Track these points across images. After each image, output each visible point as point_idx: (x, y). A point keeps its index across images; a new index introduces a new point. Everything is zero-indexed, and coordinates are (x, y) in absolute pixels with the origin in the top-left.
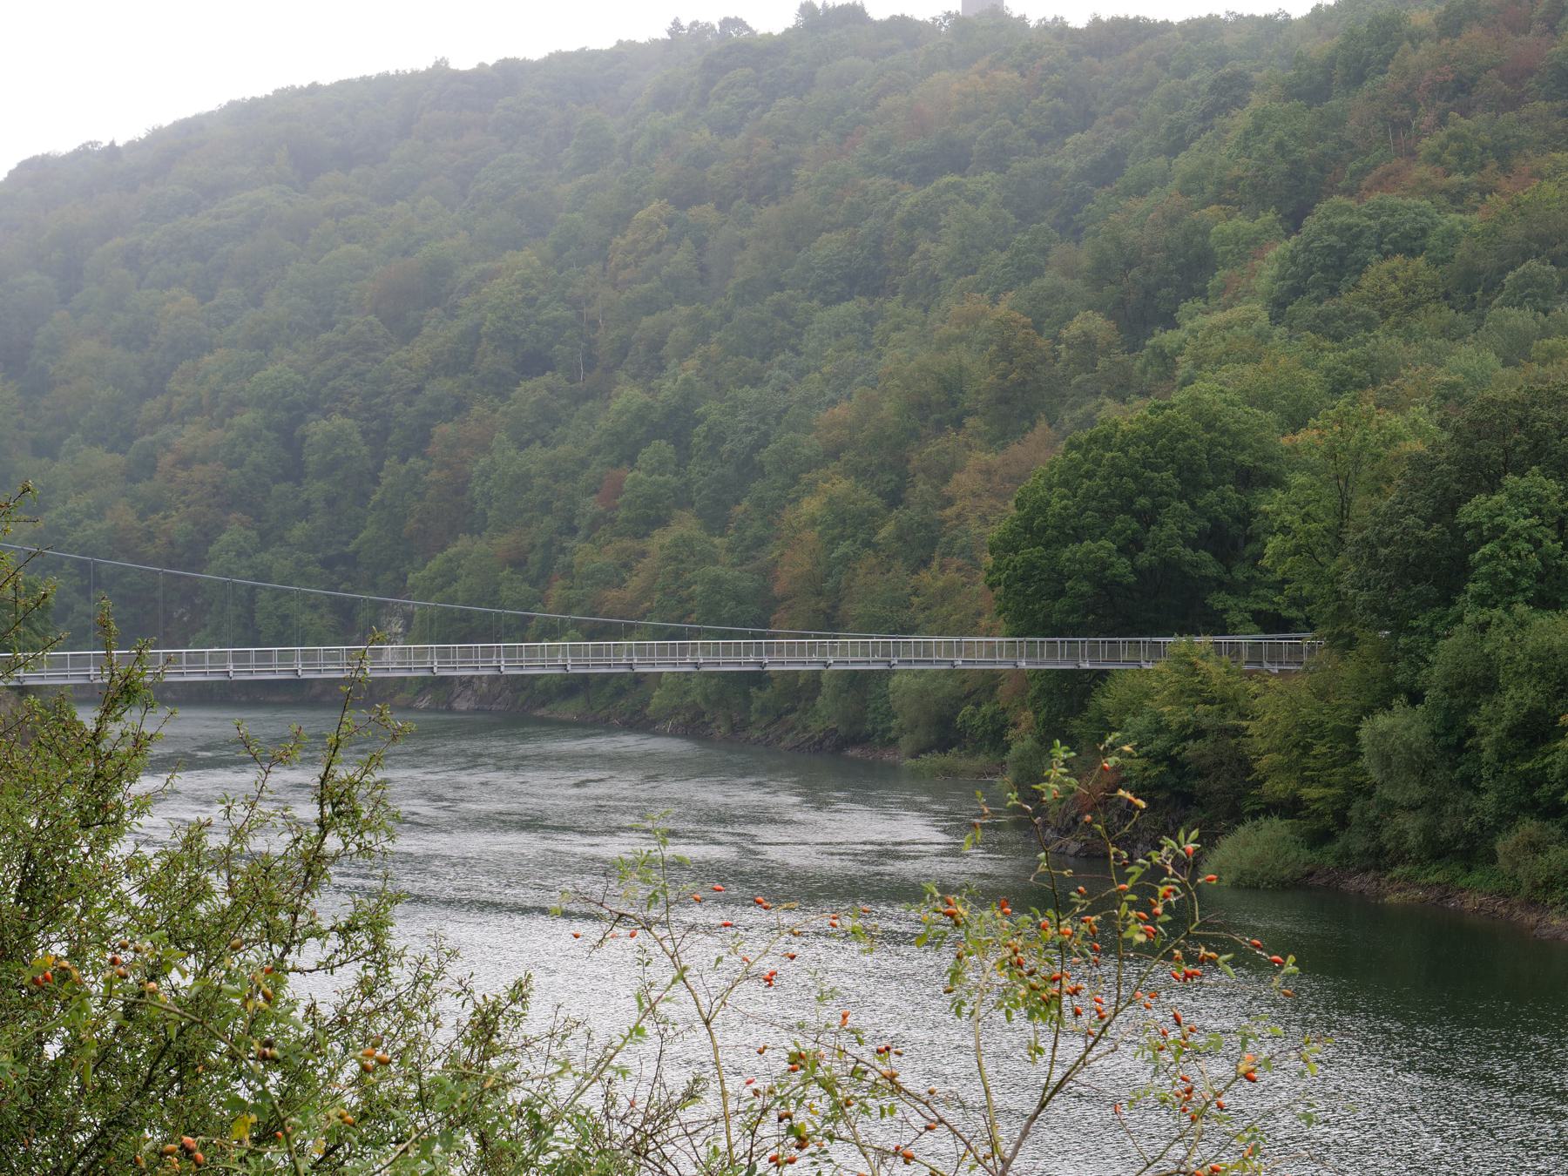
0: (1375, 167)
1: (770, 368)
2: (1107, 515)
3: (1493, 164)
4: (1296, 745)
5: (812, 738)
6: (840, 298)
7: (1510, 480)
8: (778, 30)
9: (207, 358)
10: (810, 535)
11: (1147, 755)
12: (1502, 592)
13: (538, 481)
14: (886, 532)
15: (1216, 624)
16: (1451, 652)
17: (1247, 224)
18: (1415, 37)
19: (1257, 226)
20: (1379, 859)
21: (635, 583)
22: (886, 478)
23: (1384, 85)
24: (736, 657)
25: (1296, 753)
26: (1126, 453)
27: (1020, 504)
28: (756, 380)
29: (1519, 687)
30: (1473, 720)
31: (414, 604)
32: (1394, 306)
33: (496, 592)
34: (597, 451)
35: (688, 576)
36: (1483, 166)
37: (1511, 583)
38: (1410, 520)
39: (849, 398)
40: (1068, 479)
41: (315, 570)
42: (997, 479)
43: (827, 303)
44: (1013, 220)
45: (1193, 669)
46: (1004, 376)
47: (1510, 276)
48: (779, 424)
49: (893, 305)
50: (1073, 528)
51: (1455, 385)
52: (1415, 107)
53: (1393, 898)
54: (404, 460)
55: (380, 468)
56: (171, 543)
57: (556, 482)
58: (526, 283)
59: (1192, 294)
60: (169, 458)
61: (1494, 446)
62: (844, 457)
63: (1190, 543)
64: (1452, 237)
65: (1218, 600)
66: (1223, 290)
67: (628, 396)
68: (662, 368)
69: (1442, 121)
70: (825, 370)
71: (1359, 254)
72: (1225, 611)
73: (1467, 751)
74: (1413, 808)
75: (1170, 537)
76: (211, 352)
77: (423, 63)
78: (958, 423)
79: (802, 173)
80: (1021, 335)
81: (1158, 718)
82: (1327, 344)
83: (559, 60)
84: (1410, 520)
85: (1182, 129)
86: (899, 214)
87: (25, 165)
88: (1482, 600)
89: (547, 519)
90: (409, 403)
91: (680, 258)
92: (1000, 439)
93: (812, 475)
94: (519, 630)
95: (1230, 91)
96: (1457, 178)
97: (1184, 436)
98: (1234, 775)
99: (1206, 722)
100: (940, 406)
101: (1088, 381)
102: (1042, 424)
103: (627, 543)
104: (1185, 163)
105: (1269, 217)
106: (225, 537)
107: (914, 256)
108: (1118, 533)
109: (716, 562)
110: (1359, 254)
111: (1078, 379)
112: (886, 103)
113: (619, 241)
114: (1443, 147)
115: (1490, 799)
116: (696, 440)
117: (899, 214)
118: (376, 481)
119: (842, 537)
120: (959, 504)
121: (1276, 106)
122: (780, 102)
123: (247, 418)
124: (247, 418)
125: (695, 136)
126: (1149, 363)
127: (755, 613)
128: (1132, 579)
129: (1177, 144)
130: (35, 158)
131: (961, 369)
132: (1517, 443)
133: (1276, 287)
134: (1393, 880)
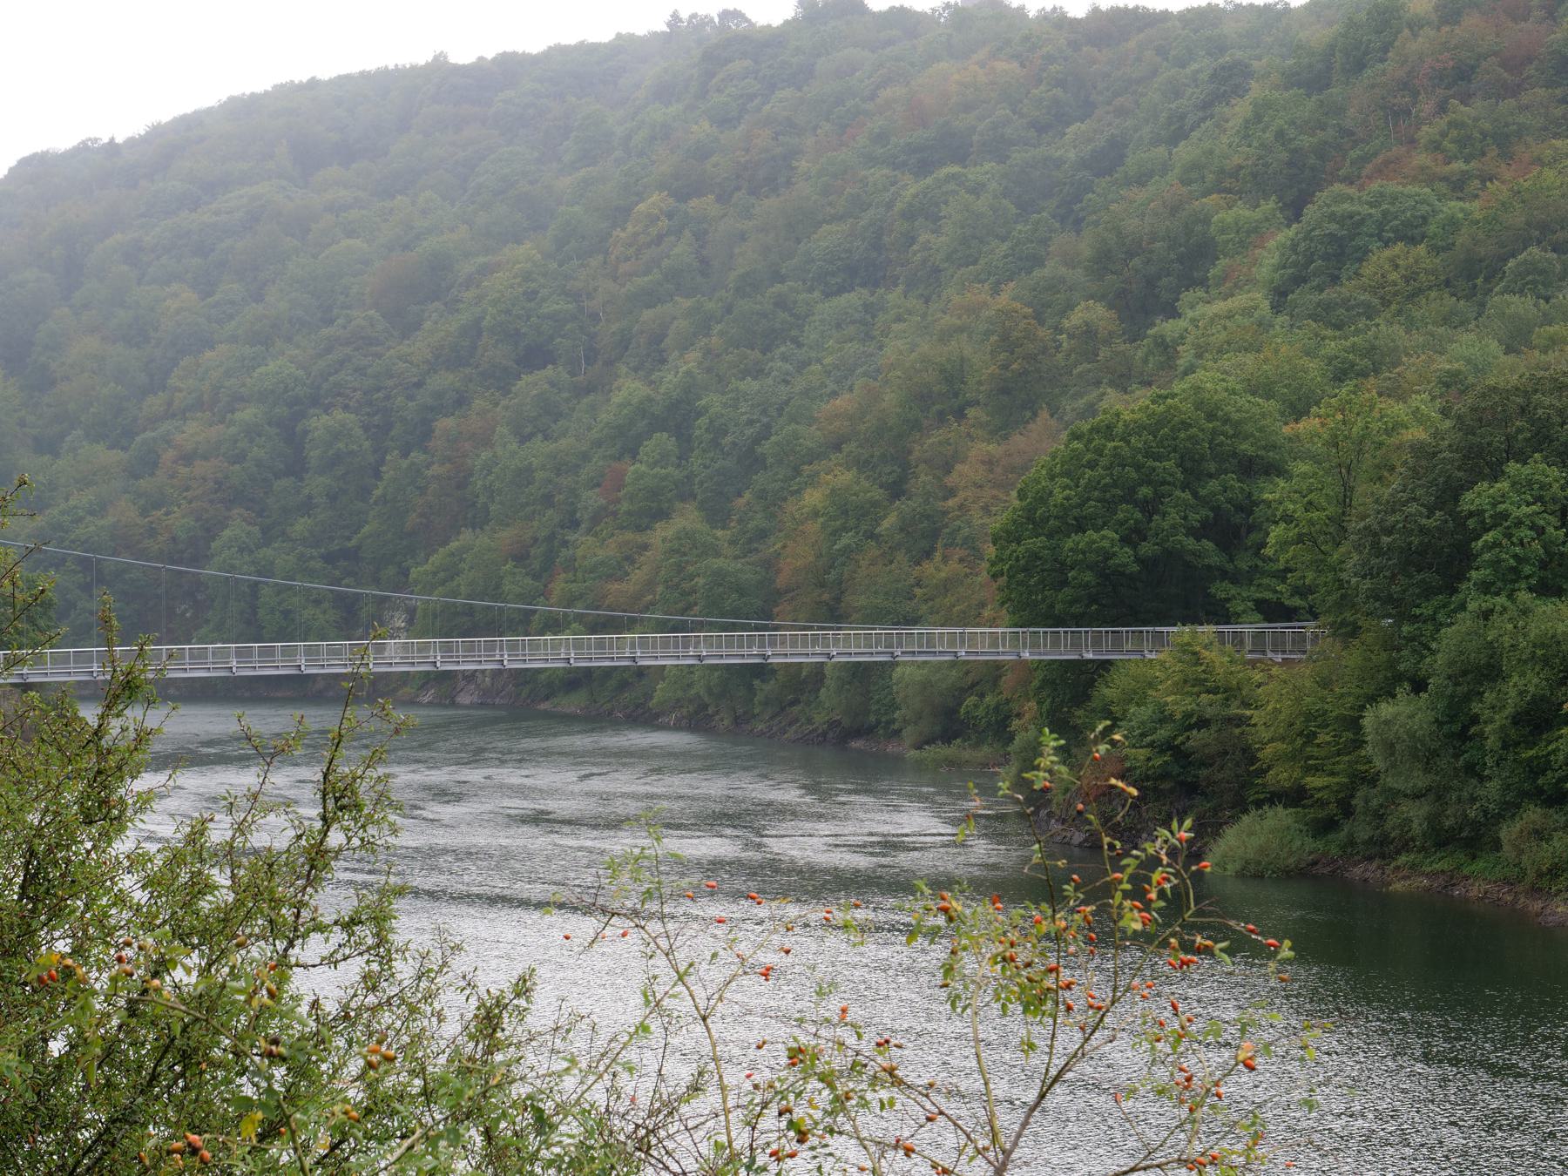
0: (1376, 154)
1: (772, 360)
2: (1110, 505)
3: (1493, 152)
4: (1300, 734)
5: (815, 730)
6: (840, 291)
7: (1512, 467)
8: (776, 21)
9: (209, 354)
10: (813, 527)
11: (1151, 745)
12: (1507, 578)
13: (540, 475)
14: (889, 523)
15: (1219, 613)
16: (1455, 638)
17: (1247, 213)
18: (1416, 25)
19: (1258, 214)
20: (1383, 848)
21: (638, 576)
22: (888, 469)
23: (1384, 73)
24: (741, 650)
25: (1299, 742)
26: (1128, 443)
27: (1022, 495)
28: (758, 372)
29: (1522, 674)
30: (1476, 707)
31: (417, 599)
32: (1395, 294)
33: (498, 586)
34: (598, 444)
35: (691, 569)
36: (1483, 154)
37: (1513, 569)
38: (1413, 508)
39: (851, 390)
40: (1071, 468)
41: (317, 565)
42: (999, 470)
43: (828, 295)
44: (1013, 210)
45: (1197, 659)
46: (1005, 367)
47: (1511, 263)
48: (780, 415)
49: (894, 296)
50: (1075, 519)
51: (1458, 373)
52: (1415, 94)
53: (1398, 886)
54: (405, 455)
55: (382, 462)
56: (174, 539)
57: (558, 475)
58: (527, 277)
59: (1191, 282)
60: (170, 454)
61: (1495, 434)
62: (846, 448)
63: (1192, 532)
64: (1453, 225)
65: (1220, 589)
66: (1224, 279)
67: (629, 389)
68: (663, 361)
69: (1442, 108)
70: (826, 361)
71: (1359, 242)
72: (1228, 600)
73: (1471, 738)
74: (1417, 796)
75: (1173, 527)
76: (212, 348)
77: (422, 57)
78: (960, 414)
79: (803, 165)
80: (1022, 325)
81: (1161, 708)
82: (1329, 332)
83: (558, 53)
84: (1413, 508)
85: (1182, 117)
86: (899, 206)
87: (25, 162)
88: (1485, 588)
89: (550, 512)
90: (411, 398)
91: (681, 250)
92: (1000, 431)
93: (815, 467)
94: (522, 624)
95: (1229, 81)
96: (1458, 165)
97: (1186, 425)
98: (1237, 765)
99: (1209, 712)
100: (942, 398)
101: (1089, 371)
102: (1044, 414)
103: (629, 536)
104: (1185, 152)
105: (1269, 205)
106: (227, 533)
107: (915, 247)
108: (1121, 523)
109: (718, 555)
110: (1359, 242)
111: (1079, 369)
112: (886, 93)
113: (617, 232)
114: (1444, 135)
115: (1493, 787)
116: (697, 432)
117: (899, 206)
118: (377, 475)
119: (845, 529)
120: (962, 494)
121: (1276, 94)
122: (780, 94)
123: (248, 414)
124: (247, 414)
125: (695, 128)
126: (1150, 352)
127: (758, 606)
128: (1135, 568)
129: (1177, 133)
130: (35, 155)
131: (962, 359)
132: (1519, 431)
133: (1277, 276)
134: (1397, 868)
